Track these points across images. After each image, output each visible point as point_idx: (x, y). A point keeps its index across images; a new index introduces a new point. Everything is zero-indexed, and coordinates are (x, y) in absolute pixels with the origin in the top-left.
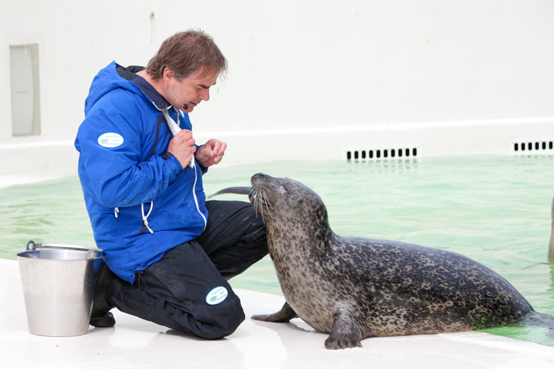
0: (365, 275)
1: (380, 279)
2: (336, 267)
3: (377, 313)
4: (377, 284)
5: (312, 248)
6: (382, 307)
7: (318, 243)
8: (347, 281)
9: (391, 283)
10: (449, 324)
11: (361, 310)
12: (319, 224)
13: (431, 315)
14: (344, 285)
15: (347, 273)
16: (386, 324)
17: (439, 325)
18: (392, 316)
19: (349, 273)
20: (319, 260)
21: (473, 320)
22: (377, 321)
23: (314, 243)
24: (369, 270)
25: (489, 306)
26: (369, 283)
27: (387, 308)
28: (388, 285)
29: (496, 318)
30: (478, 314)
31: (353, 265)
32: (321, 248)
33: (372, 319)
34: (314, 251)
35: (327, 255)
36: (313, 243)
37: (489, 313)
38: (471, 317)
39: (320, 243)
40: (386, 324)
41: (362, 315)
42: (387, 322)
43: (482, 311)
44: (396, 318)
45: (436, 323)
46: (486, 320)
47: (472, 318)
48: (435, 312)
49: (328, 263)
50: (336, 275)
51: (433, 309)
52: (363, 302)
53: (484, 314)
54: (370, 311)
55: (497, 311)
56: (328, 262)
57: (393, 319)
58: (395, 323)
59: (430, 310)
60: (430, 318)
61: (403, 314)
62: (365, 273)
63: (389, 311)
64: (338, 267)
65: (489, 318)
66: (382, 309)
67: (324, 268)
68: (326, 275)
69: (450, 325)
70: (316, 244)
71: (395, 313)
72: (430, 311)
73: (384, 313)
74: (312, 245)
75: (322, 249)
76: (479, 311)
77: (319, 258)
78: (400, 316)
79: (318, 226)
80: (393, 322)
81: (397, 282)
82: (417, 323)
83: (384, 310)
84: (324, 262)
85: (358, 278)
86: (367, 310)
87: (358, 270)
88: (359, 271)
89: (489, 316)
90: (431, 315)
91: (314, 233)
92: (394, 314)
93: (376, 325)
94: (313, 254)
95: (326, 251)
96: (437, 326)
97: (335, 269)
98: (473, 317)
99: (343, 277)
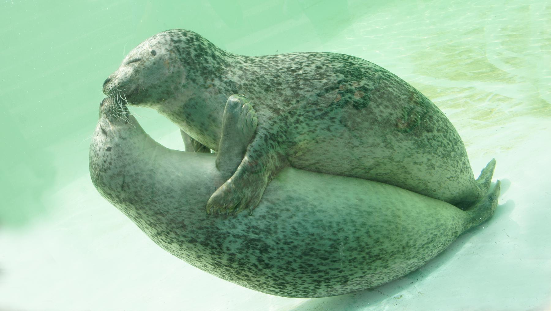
0: (275, 79)
1: (295, 79)
2: (240, 77)
3: (301, 118)
4: (293, 86)
5: (201, 71)
6: (308, 109)
7: (203, 62)
8: (256, 89)
9: (311, 81)
10: (400, 141)
11: (280, 120)
12: (188, 46)
13: (379, 123)
14: (254, 94)
15: (255, 81)
16: (315, 130)
17: (389, 141)
18: (323, 120)
19: (257, 80)
20: (216, 77)
21: (427, 145)
22: (303, 128)
23: (199, 65)
24: (279, 74)
25: (449, 138)
26: (282, 86)
27: (314, 110)
28: (307, 82)
29: (455, 155)
30: (435, 140)
31: (259, 72)
32: (210, 64)
33: (296, 128)
34: (205, 71)
35: (223, 67)
36: (198, 67)
37: (449, 146)
38: (426, 140)
39: (206, 59)
40: (315, 130)
41: (281, 127)
42: (316, 128)
43: (440, 139)
44: (329, 123)
45: (385, 136)
46: (443, 152)
47: (427, 143)
48: (384, 119)
49: (230, 75)
50: (242, 85)
51: (382, 114)
52: (279, 109)
53: (443, 145)
54: (292, 117)
55: (456, 147)
56: (228, 74)
57: (325, 123)
58: (328, 129)
59: (377, 115)
60: (377, 127)
61: (339, 117)
62: (275, 77)
63: (318, 113)
64: (242, 75)
65: (447, 151)
66: (308, 112)
67: (226, 83)
68: (230, 89)
69: (401, 143)
70: (202, 63)
71: (328, 116)
72: (377, 117)
73: (311, 116)
74: (199, 69)
75: (212, 64)
76: (437, 137)
77: (215, 74)
78: (334, 120)
79: (188, 48)
80: (325, 128)
81: (319, 78)
82: (359, 132)
83: (310, 114)
84: (224, 76)
85: (269, 84)
86: (287, 117)
87: (266, 76)
88: (269, 77)
89: (448, 149)
90: (379, 123)
91: (190, 58)
92: (327, 118)
93: (302, 134)
94: (206, 75)
95: (218, 63)
96: (385, 142)
97: (239, 79)
98: (428, 142)
99: (250, 85)
